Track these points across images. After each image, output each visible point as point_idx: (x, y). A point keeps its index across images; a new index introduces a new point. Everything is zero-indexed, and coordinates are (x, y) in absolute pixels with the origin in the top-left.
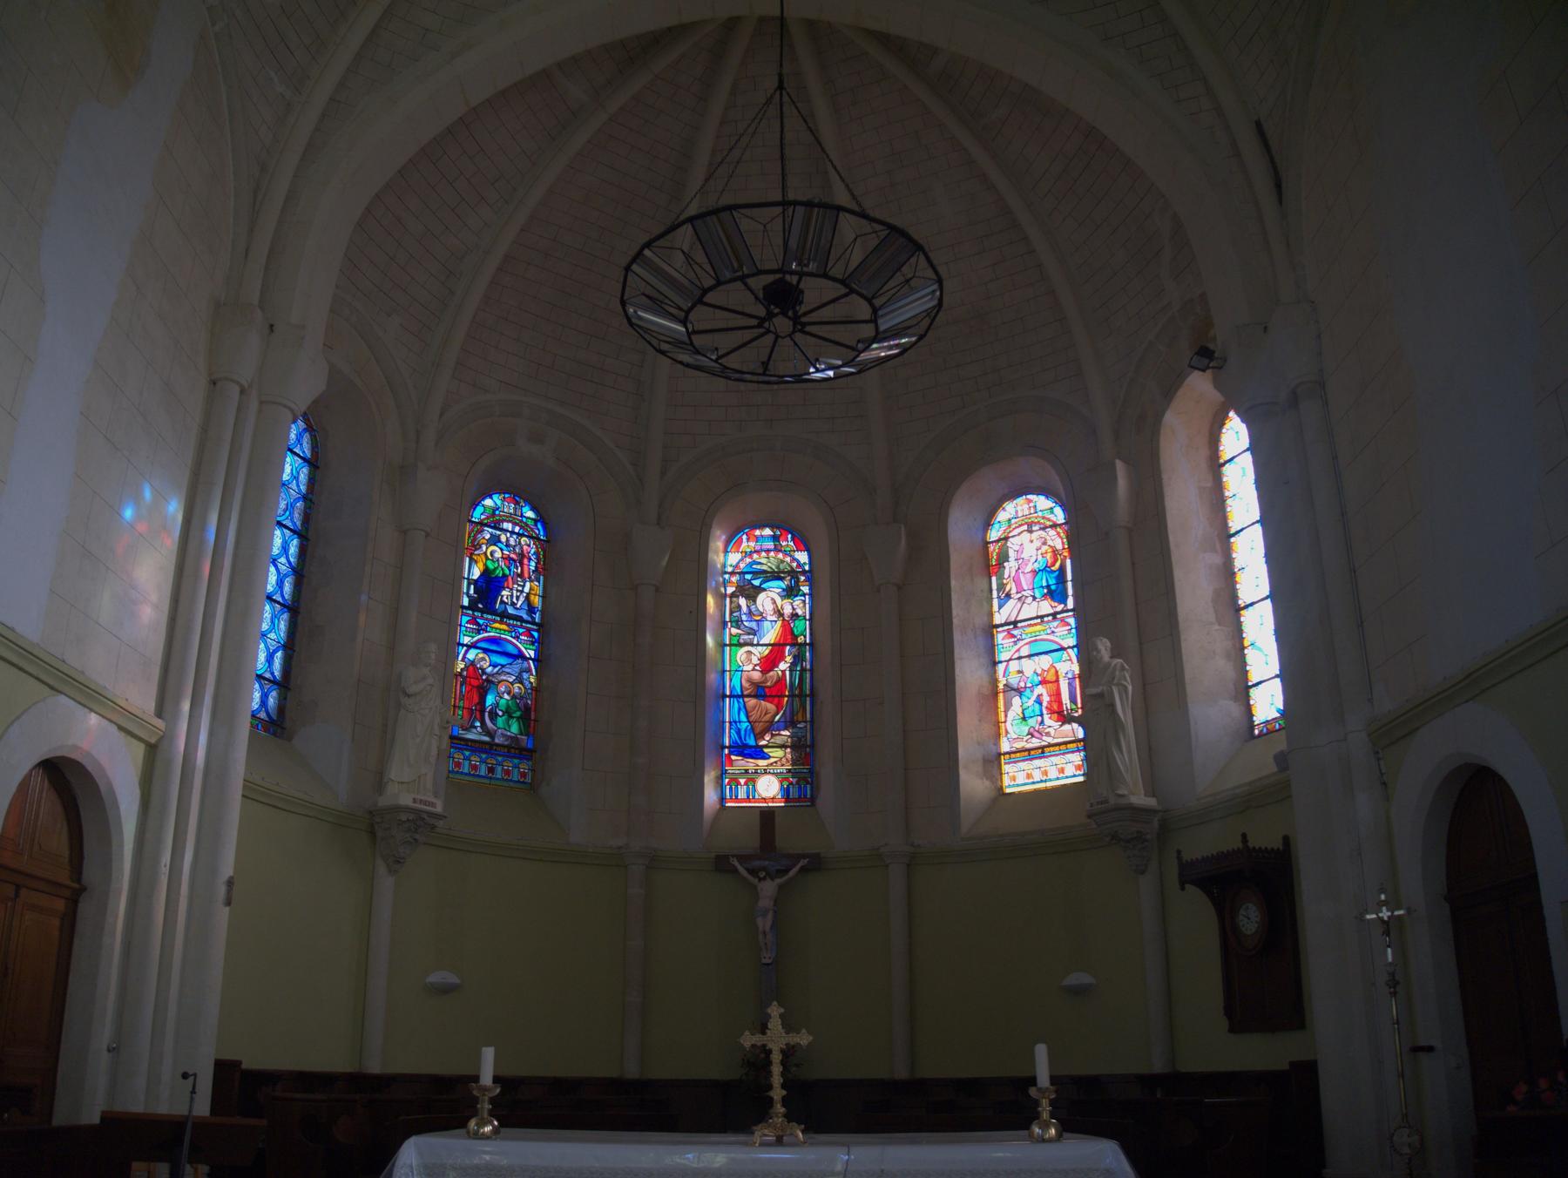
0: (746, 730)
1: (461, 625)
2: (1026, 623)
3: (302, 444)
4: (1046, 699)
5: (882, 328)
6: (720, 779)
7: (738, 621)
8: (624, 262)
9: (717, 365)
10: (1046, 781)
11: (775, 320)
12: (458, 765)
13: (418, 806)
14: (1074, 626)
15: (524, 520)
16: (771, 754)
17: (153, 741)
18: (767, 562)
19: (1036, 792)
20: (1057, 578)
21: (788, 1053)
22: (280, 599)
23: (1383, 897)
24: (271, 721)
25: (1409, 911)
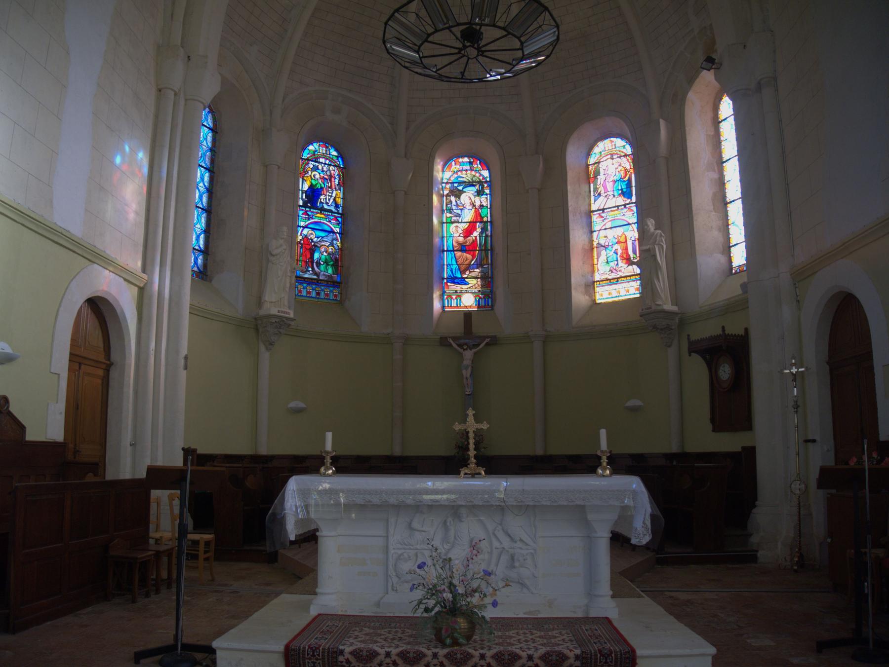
0: (455, 269)
1: (299, 216)
2: (609, 210)
3: (207, 120)
4: (620, 252)
5: (526, 53)
6: (442, 296)
7: (450, 210)
8: (385, 19)
9: (436, 74)
10: (619, 296)
11: (468, 49)
12: (300, 291)
13: (280, 314)
14: (635, 211)
15: (331, 156)
16: (469, 282)
17: (142, 285)
18: (467, 177)
19: (614, 302)
20: (627, 184)
21: (478, 434)
22: (201, 206)
23: (793, 361)
24: (200, 272)
25: (807, 369)
